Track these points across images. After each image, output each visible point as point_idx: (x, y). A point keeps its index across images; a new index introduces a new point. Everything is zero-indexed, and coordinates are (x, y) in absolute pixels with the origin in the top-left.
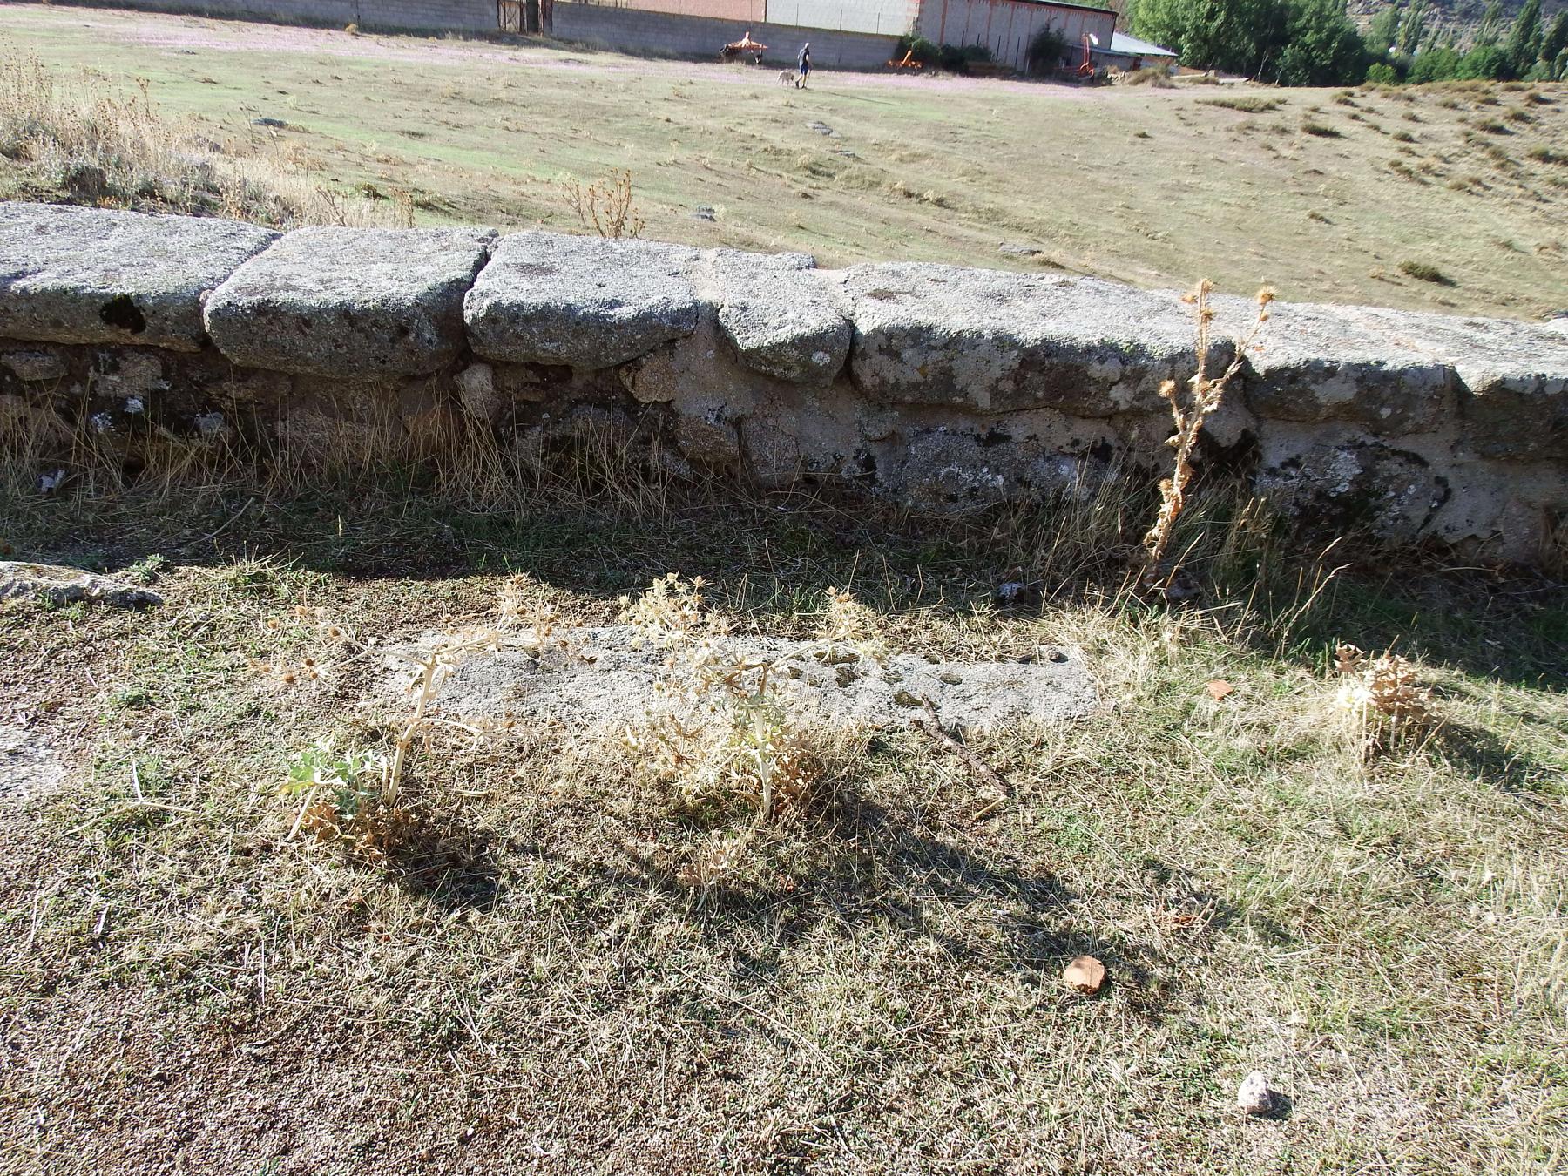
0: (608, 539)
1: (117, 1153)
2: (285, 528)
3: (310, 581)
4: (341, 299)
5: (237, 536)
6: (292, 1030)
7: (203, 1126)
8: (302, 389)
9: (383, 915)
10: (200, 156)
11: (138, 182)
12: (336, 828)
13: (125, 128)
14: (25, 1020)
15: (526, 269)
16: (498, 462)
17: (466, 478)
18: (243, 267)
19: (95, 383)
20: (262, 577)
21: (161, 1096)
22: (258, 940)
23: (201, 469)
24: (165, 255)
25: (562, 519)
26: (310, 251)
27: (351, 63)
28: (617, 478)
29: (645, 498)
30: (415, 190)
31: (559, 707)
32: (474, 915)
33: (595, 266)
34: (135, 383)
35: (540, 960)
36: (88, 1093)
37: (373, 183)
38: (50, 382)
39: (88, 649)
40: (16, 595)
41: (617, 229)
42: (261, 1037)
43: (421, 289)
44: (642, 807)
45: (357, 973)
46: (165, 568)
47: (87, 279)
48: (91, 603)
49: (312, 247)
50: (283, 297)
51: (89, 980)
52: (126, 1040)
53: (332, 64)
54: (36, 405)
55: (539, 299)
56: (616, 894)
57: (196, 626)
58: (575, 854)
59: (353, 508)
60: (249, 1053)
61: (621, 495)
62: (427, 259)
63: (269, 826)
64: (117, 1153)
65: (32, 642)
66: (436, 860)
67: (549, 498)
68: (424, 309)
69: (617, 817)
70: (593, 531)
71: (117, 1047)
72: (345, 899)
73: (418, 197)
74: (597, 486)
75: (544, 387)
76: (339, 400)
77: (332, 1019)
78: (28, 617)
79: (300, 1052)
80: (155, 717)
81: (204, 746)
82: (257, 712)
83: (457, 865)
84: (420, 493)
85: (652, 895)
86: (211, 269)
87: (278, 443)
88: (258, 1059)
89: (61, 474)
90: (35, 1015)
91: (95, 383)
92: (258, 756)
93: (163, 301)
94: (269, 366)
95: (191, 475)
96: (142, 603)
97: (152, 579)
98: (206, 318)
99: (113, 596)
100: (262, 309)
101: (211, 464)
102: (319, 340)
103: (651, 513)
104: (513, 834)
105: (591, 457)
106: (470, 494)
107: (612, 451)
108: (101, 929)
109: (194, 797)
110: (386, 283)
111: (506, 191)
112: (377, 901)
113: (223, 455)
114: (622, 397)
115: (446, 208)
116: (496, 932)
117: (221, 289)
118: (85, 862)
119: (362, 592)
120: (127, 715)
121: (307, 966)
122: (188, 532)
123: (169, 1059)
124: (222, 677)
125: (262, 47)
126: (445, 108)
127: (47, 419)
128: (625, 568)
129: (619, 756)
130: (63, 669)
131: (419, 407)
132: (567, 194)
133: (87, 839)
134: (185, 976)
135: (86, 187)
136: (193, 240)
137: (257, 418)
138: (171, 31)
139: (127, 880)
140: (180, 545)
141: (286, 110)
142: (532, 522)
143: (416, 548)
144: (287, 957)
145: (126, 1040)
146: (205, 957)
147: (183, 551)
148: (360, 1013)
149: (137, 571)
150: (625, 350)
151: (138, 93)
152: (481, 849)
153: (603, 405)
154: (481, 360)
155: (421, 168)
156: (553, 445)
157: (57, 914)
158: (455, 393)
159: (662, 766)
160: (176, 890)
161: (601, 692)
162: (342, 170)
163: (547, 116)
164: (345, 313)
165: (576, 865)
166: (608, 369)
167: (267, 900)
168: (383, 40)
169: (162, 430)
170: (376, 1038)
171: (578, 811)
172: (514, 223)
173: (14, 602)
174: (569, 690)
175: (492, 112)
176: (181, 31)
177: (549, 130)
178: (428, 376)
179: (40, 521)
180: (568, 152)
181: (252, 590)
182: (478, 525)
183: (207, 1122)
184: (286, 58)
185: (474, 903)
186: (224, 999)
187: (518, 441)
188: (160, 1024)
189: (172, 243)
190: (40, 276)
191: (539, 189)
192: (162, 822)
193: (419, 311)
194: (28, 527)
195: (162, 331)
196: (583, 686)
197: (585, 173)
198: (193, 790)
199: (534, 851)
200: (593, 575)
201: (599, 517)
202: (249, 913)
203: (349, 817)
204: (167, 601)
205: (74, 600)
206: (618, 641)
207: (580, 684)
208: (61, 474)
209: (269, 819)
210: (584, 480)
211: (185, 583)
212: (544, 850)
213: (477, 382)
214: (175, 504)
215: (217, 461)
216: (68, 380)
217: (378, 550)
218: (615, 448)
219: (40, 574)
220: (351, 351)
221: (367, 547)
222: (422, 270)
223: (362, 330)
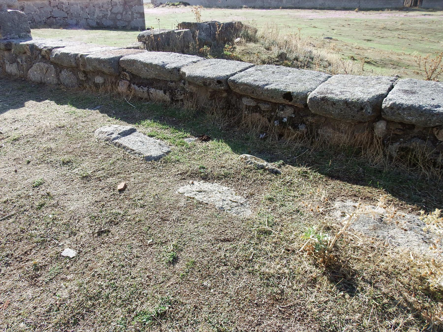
0: (415, 184)
1: (243, 320)
2: (315, 159)
3: (319, 176)
4: (345, 98)
5: (302, 159)
6: (290, 307)
7: (263, 323)
8: (328, 121)
9: (320, 284)
10: (310, 48)
11: (294, 56)
12: (313, 253)
13: (294, 42)
14: (231, 274)
15: (406, 92)
16: (382, 153)
17: (370, 155)
18: (320, 86)
19: (277, 113)
20: (306, 172)
21: (255, 309)
22: (287, 277)
23: (297, 139)
24: (300, 81)
25: (399, 174)
26: (339, 82)
27: (354, 20)
28: (423, 164)
29: (432, 172)
30: (366, 58)
31: (387, 237)
32: (347, 296)
33: (431, 92)
34: (286, 114)
35: (366, 321)
36: (240, 300)
37: (353, 55)
38: (267, 111)
39: (262, 182)
40: (250, 164)
41: (433, 72)
42: (282, 305)
43: (370, 96)
44: (412, 283)
45: (310, 298)
46: (283, 164)
47: (281, 87)
48: (265, 170)
49: (339, 81)
50: (330, 96)
51: (246, 270)
52: (251, 290)
53: (349, 21)
54: (263, 116)
55: (410, 103)
56: (397, 310)
57: (288, 182)
58: (384, 290)
59: (334, 157)
60: (278, 308)
61: (423, 170)
62: (373, 86)
63: (295, 245)
64: (243, 320)
65: (251, 177)
66: (340, 274)
67: (396, 166)
68: (370, 103)
69: (402, 283)
70: (410, 180)
71: (248, 291)
72: (311, 275)
73: (366, 60)
74: (414, 165)
75: (403, 131)
76: (337, 125)
77: (301, 309)
78: (251, 170)
79: (290, 314)
80: (274, 205)
81: (284, 217)
82: (298, 211)
83: (345, 278)
84: (355, 157)
85: (410, 317)
86: (312, 86)
87: (318, 135)
88: (280, 311)
89: (265, 134)
90: (234, 274)
91: (277, 113)
92: (296, 224)
93: (298, 94)
94: (321, 114)
95: (294, 140)
96: (277, 173)
97: (280, 167)
98: (308, 100)
99: (270, 169)
100: (323, 99)
101: (300, 138)
102: (336, 109)
103: (434, 178)
104: (364, 275)
105: (415, 155)
106: (370, 160)
107: (423, 155)
108: (251, 258)
109: (278, 230)
110: (359, 94)
111: (395, 58)
112: (320, 280)
113: (303, 136)
114: (432, 137)
115: (374, 63)
116: (353, 304)
117: (313, 92)
118: (252, 238)
119: (332, 183)
120: (268, 202)
121: (297, 290)
122: (290, 155)
123: (259, 300)
124: (291, 198)
125: (330, 17)
126: (380, 32)
127: (265, 120)
128: (420, 195)
129: (406, 262)
130: (256, 185)
131: (360, 131)
132: (416, 59)
133: (253, 232)
134: (267, 279)
135: (282, 59)
136: (308, 77)
137: (314, 127)
138: (308, 14)
139: (259, 247)
140: (288, 159)
141: (333, 34)
142: (389, 173)
143: (350, 173)
144: (293, 285)
145: (251, 290)
146: (273, 276)
147: (288, 160)
148: (309, 311)
149: (277, 164)
150: (438, 122)
151: (298, 31)
152: (353, 275)
153: (424, 139)
154: (384, 119)
155: (369, 51)
156: (402, 149)
157: (243, 249)
158: (373, 129)
159: (424, 272)
160: (270, 254)
161: (403, 236)
162: (345, 52)
163: (414, 33)
164: (346, 102)
165: (384, 294)
166: (429, 128)
167: (291, 266)
168: (365, 12)
169: (290, 127)
170: (312, 321)
171: (388, 275)
172: (395, 68)
173: (249, 166)
174: (392, 232)
175: (395, 33)
176: (311, 14)
177: (413, 38)
178: (365, 122)
179: (258, 146)
180: (419, 45)
181: (303, 176)
182: (371, 170)
183: (265, 322)
184: (336, 20)
185: (348, 292)
186: (275, 290)
187: (390, 146)
188: (259, 289)
189: (303, 78)
190: (271, 85)
191: (406, 57)
192: (270, 234)
193: (368, 103)
194: (255, 146)
195: (296, 102)
196: (397, 232)
197: (423, 51)
198: (279, 228)
199: (371, 283)
200: (407, 195)
201: (413, 175)
202: (286, 268)
203: (317, 251)
204: (282, 173)
205: (262, 168)
206: (412, 220)
207: (395, 232)
208: (265, 134)
209: (296, 243)
210: (410, 162)
211: (287, 170)
212: (374, 284)
213: (381, 126)
214: (289, 147)
215: (301, 137)
216: (272, 111)
217: (339, 171)
218: (425, 154)
219: (256, 160)
220: (345, 113)
221: (336, 170)
222: (371, 90)
223: (350, 107)
